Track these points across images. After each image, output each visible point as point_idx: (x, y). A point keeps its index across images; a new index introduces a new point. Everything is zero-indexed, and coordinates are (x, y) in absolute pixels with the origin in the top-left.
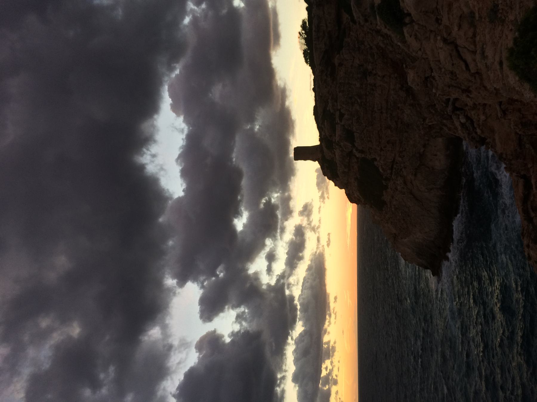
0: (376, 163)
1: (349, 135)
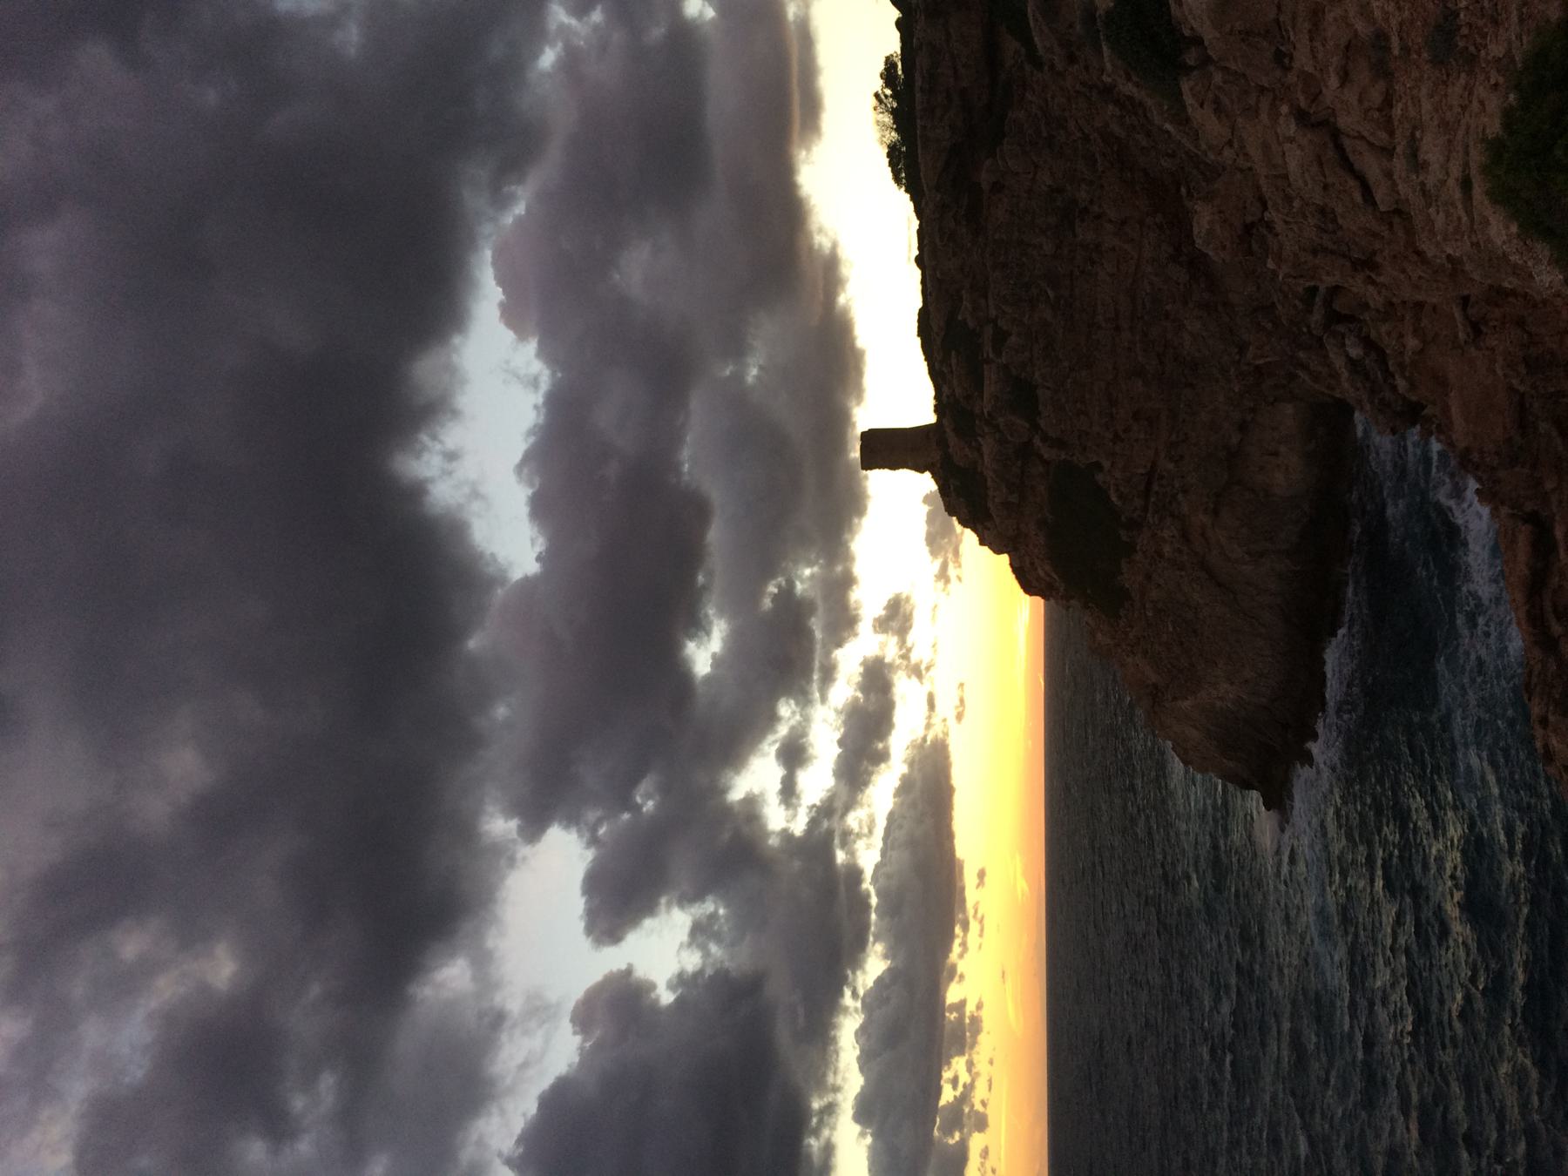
0: (1100, 477)
1: (1023, 396)
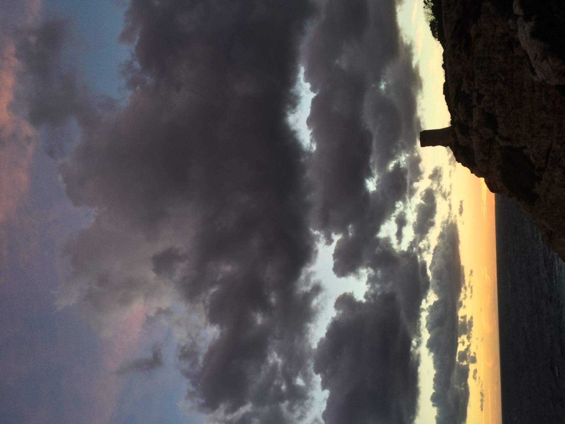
0: (525, 151)
1: (490, 120)
